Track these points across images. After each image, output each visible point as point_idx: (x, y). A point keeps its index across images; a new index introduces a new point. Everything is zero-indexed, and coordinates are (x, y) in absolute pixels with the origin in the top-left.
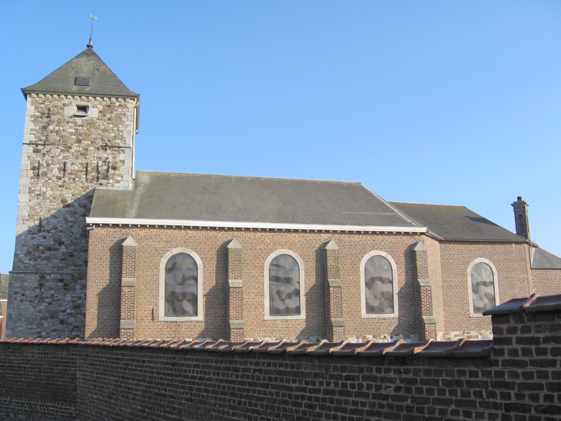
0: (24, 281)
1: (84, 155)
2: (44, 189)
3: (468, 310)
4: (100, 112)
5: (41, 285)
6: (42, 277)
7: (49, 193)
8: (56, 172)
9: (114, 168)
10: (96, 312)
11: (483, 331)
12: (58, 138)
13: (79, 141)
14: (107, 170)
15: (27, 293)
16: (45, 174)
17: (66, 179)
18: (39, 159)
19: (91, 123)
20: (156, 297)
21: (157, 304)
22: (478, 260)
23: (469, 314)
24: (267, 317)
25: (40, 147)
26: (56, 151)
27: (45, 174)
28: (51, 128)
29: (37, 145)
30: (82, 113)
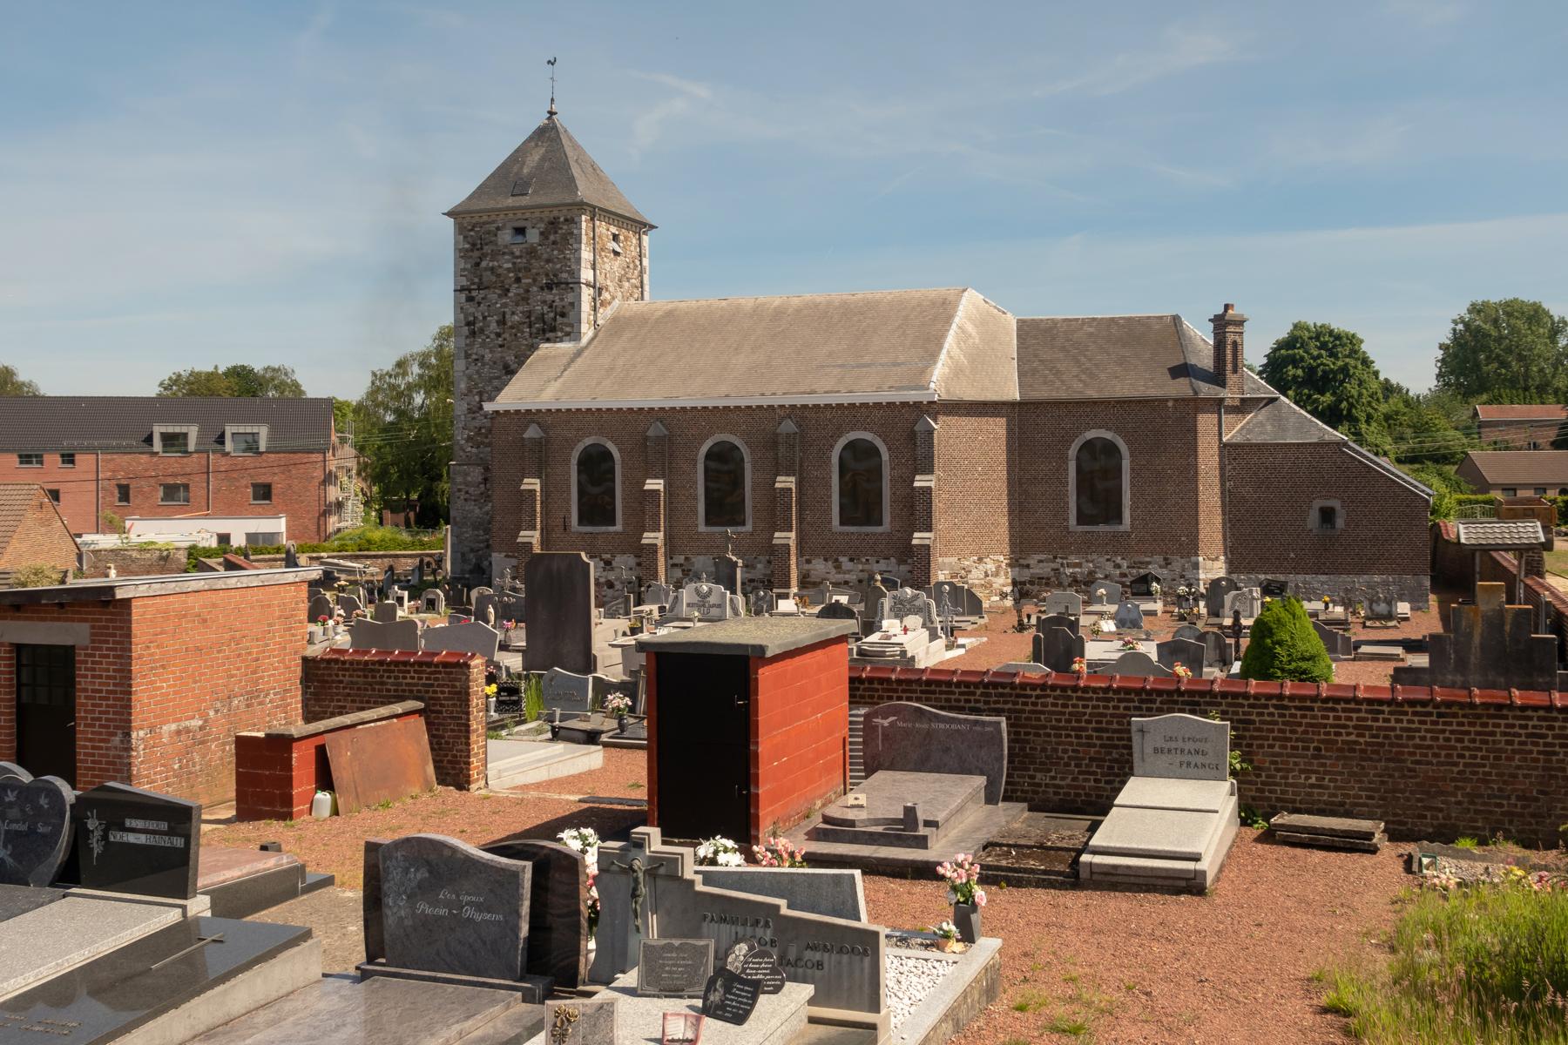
0: (467, 474)
1: (526, 300)
2: (481, 351)
3: (1066, 520)
4: (542, 233)
5: (486, 480)
6: (487, 469)
7: (488, 356)
8: (493, 326)
9: (563, 315)
10: (1201, 497)
11: (1095, 556)
12: (494, 279)
13: (518, 280)
14: (555, 319)
15: (471, 490)
16: (482, 330)
17: (506, 335)
18: (472, 310)
19: (532, 252)
20: (568, 501)
21: (569, 511)
22: (1091, 434)
23: (1067, 527)
24: (702, 528)
25: (474, 294)
26: (493, 296)
27: (482, 330)
28: (484, 264)
29: (470, 290)
30: (519, 239)
